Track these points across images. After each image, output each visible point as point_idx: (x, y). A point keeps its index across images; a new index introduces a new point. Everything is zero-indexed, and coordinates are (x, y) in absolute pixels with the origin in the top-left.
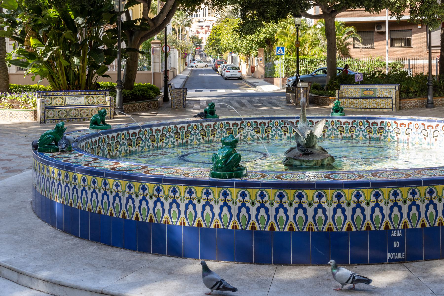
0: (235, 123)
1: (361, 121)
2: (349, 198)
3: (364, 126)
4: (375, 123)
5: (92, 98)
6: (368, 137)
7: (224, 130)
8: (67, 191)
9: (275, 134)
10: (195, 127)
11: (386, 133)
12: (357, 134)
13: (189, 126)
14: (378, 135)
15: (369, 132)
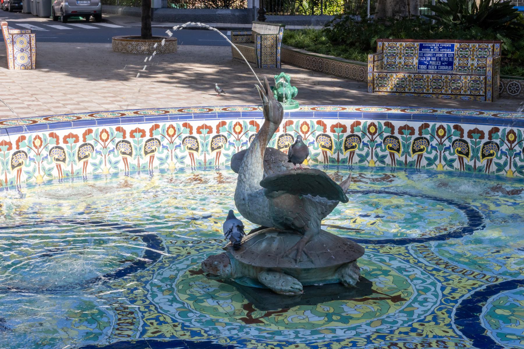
1: (441, 127)
3: (449, 138)
4: (476, 131)
6: (388, 160)
9: (367, 155)
10: (171, 132)
11: (434, 152)
12: (432, 156)
14: (414, 157)
15: (391, 149)
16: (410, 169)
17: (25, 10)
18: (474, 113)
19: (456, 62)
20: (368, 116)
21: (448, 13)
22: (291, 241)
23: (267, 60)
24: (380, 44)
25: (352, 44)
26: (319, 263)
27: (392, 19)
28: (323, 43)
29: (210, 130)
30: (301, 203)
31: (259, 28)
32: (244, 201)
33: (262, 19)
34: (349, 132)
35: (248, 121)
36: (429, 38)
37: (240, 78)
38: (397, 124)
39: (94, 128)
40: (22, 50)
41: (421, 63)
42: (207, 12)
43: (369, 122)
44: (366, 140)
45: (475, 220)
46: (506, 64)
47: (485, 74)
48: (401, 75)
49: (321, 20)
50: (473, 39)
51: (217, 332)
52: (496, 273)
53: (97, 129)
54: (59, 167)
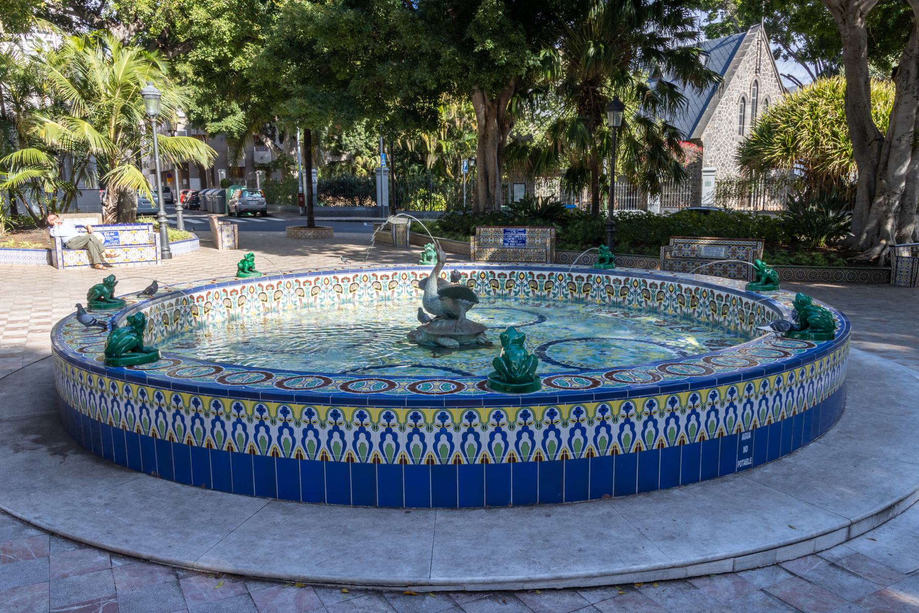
2: (375, 420)
6: (492, 293)
10: (561, 278)
14: (546, 292)
16: (505, 297)
17: (202, 207)
18: (540, 265)
19: (527, 241)
20: (480, 268)
21: (521, 209)
22: (452, 323)
23: (400, 241)
24: (478, 229)
25: (458, 231)
26: (466, 332)
27: (484, 213)
28: (437, 230)
29: (388, 277)
30: (456, 303)
31: (392, 220)
32: (428, 302)
33: (394, 213)
34: (469, 278)
35: (410, 272)
36: (508, 225)
37: (384, 254)
38: (497, 272)
39: (320, 277)
40: (228, 236)
41: (505, 242)
42: (346, 209)
43: (481, 271)
44: (479, 282)
45: (542, 319)
46: (559, 243)
47: (546, 248)
48: (493, 250)
49: (432, 214)
50: (538, 226)
51: (630, 19)
52: (553, 336)
53: (322, 277)
54: (300, 300)
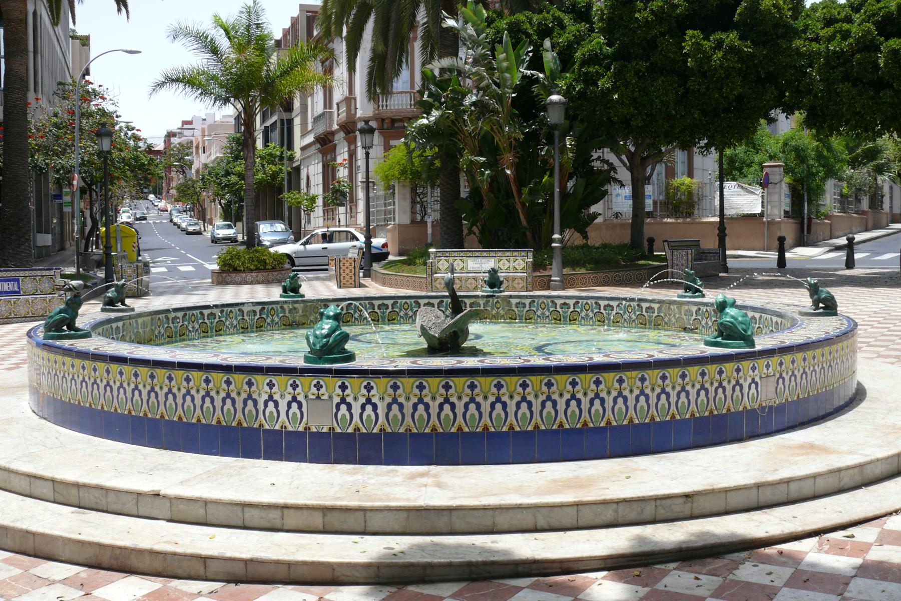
0: (565, 304)
4: (609, 305)
5: (506, 262)
7: (547, 313)
8: (73, 386)
13: (263, 309)
